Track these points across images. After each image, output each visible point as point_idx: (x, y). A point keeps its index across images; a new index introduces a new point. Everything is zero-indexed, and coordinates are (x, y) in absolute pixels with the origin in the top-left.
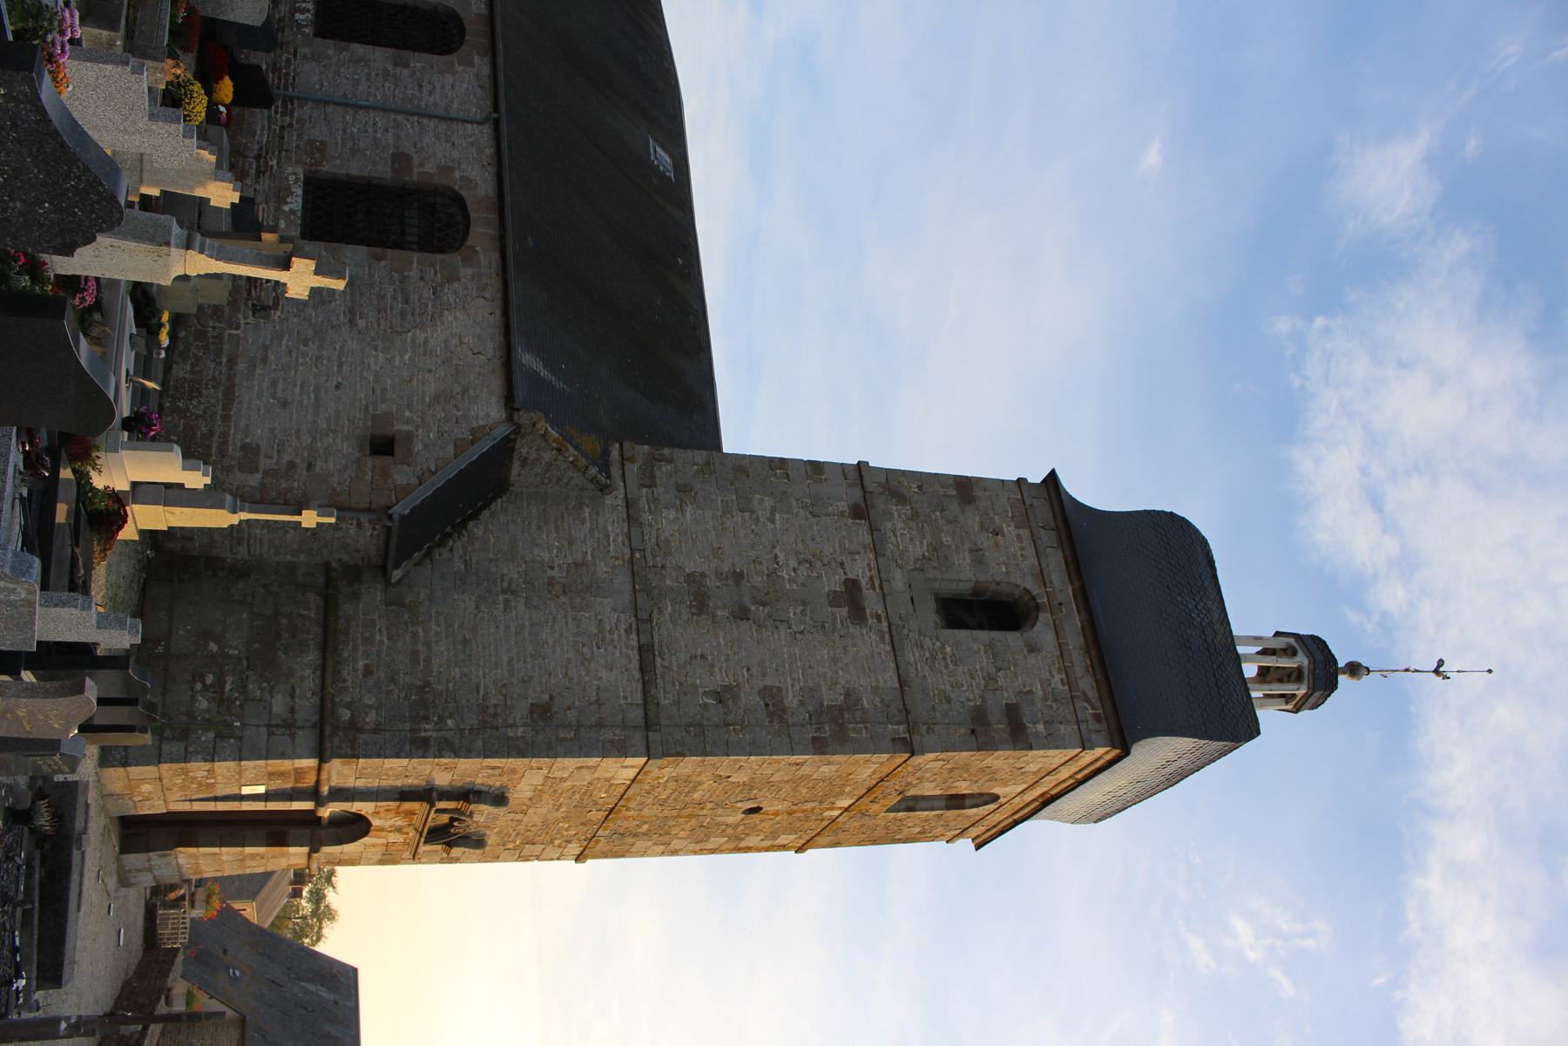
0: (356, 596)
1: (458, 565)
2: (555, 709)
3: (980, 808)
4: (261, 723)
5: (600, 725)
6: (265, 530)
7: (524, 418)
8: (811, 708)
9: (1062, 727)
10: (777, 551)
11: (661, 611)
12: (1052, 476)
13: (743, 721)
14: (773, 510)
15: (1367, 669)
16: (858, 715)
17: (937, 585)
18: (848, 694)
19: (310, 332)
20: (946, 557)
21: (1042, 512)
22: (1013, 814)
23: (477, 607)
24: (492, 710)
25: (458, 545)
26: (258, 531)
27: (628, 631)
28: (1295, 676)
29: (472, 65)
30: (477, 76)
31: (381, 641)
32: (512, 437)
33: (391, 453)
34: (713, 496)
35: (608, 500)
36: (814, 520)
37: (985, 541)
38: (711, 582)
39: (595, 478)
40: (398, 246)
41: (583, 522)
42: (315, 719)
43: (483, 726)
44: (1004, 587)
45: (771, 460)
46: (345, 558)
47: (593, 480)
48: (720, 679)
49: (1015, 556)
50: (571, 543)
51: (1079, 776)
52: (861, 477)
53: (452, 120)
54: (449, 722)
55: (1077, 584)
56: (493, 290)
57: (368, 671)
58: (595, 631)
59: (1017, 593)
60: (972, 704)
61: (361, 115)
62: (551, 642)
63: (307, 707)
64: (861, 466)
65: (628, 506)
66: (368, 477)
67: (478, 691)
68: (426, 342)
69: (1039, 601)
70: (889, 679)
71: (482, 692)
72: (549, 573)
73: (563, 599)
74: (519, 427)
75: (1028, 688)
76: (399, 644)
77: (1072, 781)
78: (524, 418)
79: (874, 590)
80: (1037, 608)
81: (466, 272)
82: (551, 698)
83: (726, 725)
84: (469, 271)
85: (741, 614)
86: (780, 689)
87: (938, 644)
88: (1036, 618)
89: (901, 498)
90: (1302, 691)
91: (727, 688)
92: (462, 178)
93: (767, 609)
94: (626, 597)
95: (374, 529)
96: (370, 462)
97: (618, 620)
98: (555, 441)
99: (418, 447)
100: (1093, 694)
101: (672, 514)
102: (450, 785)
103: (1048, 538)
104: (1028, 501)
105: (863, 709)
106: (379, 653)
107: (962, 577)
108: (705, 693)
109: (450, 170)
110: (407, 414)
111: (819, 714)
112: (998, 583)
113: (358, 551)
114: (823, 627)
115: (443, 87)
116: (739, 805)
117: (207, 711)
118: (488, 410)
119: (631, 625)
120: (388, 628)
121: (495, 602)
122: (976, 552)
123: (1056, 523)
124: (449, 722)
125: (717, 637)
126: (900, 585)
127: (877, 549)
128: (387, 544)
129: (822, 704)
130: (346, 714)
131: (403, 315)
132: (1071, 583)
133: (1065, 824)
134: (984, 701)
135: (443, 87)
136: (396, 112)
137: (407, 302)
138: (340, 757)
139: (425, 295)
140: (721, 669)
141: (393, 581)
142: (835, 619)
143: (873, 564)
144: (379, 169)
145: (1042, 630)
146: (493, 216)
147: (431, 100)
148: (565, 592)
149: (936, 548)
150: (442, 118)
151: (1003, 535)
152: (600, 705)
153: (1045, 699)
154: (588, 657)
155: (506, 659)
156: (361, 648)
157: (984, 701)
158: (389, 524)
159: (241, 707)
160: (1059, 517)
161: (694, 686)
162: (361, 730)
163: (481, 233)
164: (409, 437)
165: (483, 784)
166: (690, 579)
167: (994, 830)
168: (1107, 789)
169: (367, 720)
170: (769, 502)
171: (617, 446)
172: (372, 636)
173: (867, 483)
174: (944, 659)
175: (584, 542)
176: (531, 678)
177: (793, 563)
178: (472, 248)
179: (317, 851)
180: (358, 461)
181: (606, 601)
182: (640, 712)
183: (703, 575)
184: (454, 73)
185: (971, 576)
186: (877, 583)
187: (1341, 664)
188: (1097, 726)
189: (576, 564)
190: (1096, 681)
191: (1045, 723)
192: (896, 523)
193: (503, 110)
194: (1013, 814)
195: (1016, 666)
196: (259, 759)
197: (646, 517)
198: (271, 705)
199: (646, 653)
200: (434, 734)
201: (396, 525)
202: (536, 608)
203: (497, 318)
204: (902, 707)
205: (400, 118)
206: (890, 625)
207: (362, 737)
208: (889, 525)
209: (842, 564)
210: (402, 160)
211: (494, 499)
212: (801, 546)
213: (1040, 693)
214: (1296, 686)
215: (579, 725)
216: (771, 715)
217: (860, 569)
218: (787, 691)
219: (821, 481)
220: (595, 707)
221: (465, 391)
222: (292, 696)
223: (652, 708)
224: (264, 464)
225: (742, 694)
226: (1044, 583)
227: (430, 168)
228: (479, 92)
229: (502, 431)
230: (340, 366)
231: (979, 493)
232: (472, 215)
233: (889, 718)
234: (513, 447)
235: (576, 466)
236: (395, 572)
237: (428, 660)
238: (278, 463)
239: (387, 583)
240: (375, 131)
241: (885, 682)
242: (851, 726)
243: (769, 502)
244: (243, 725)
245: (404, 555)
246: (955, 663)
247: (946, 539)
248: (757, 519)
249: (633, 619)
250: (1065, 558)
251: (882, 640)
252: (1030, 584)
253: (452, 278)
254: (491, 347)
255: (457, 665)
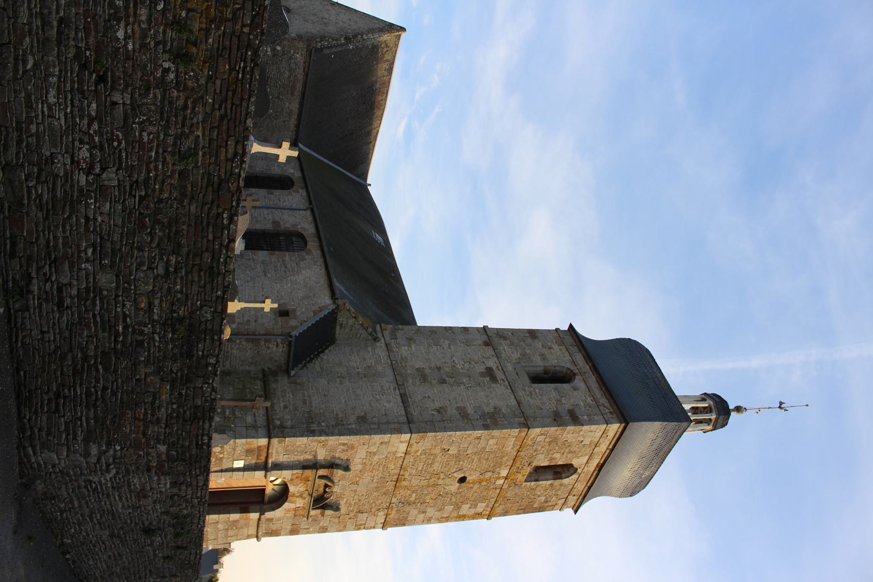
0: (276, 381)
1: (318, 369)
2: (367, 418)
3: (570, 478)
4: (242, 425)
5: (388, 423)
6: (238, 351)
7: (340, 302)
8: (480, 414)
9: (595, 417)
10: (454, 358)
11: (407, 382)
12: (571, 326)
13: (450, 419)
14: (450, 345)
15: (745, 408)
16: (501, 415)
17: (527, 369)
18: (495, 408)
19: (249, 279)
20: (529, 358)
21: (569, 340)
22: (587, 483)
23: (328, 383)
24: (340, 419)
25: (317, 362)
26: (235, 352)
27: (395, 389)
28: (707, 410)
29: (299, 192)
30: (301, 196)
31: (289, 397)
32: (336, 311)
33: (288, 315)
34: (423, 341)
35: (378, 344)
36: (468, 348)
37: (545, 351)
38: (427, 371)
39: (371, 333)
40: (281, 250)
41: (369, 352)
42: (265, 424)
43: (337, 425)
44: (558, 368)
45: (445, 328)
46: (271, 366)
47: (370, 334)
48: (437, 405)
49: (560, 356)
50: (365, 360)
51: (611, 447)
52: (486, 331)
53: (294, 209)
54: (323, 424)
55: (590, 364)
56: (320, 261)
57: (285, 407)
58: (380, 390)
59: (564, 370)
60: (552, 410)
61: (257, 210)
62: (362, 394)
63: (261, 420)
64: (485, 328)
65: (387, 345)
66: (280, 323)
67: (334, 413)
68: (296, 280)
69: (575, 372)
70: (513, 402)
71: (335, 413)
72: (357, 370)
73: (365, 379)
74: (338, 306)
75: (576, 403)
76: (297, 397)
77: (608, 451)
78: (340, 302)
79: (499, 370)
80: (574, 374)
81: (308, 257)
82: (365, 414)
83: (444, 421)
84: (310, 257)
85: (443, 381)
86: (464, 407)
87: (532, 389)
88: (575, 378)
89: (505, 338)
90: (713, 417)
91: (441, 408)
92: (301, 228)
93: (454, 379)
94: (392, 377)
95: (284, 347)
96: (280, 319)
97: (390, 386)
98: (354, 313)
99: (298, 313)
100: (607, 404)
101: (406, 348)
102: (325, 460)
103: (574, 349)
104: (562, 336)
105: (503, 413)
106: (289, 401)
107: (538, 364)
108: (432, 410)
109: (297, 225)
110: (292, 303)
111: (483, 416)
112: (555, 367)
113: (276, 361)
114: (479, 384)
115: (288, 200)
116: (455, 475)
117: (220, 421)
118: (326, 300)
119: (395, 387)
120: (291, 392)
121: (336, 381)
122: (542, 355)
123: (576, 342)
124: (323, 424)
125: (434, 390)
126: (511, 368)
127: (498, 356)
128: (289, 357)
129: (484, 412)
130: (278, 423)
131: (285, 272)
132: (588, 364)
133: (616, 498)
134: (557, 408)
135: (288, 200)
136: (271, 208)
137: (286, 268)
138: (277, 437)
139: (293, 265)
140: (437, 401)
141: (291, 375)
142: (484, 382)
143: (497, 362)
144: (269, 226)
145: (578, 381)
146: (316, 239)
147: (284, 204)
148: (365, 377)
149: (524, 355)
150: (290, 209)
151: (553, 349)
152: (387, 416)
153: (585, 407)
154: (379, 398)
155: (343, 401)
156: (281, 399)
157: (557, 408)
158: (291, 339)
159: (234, 420)
160: (577, 341)
161: (427, 408)
162: (285, 428)
163: (313, 245)
164: (295, 310)
165: (339, 458)
166: (418, 370)
167: (581, 498)
168: (629, 466)
169: (288, 424)
170: (447, 342)
171: (379, 326)
172: (285, 395)
173: (488, 333)
174: (536, 394)
175: (370, 359)
176: (355, 407)
177: (462, 362)
178: (310, 250)
179: (264, 514)
180: (275, 319)
181: (383, 379)
182: (405, 418)
183: (423, 368)
184: (292, 195)
185: (542, 364)
186: (500, 368)
187: (731, 407)
188: (612, 416)
189: (368, 367)
190: (608, 399)
191: (587, 416)
192: (505, 348)
193: (313, 203)
194: (587, 483)
195: (569, 395)
196: (243, 438)
197: (395, 349)
198: (246, 420)
199: (404, 397)
200: (317, 428)
201: (293, 340)
202: (354, 383)
203: (323, 271)
204: (520, 412)
205: (273, 210)
206: (509, 382)
207: (286, 430)
208: (502, 348)
209: (483, 362)
210: (276, 223)
211: (330, 346)
212: (464, 357)
213: (582, 404)
214: (710, 414)
215: (379, 423)
216: (463, 417)
217: (492, 363)
218: (468, 408)
219: (468, 334)
220: (384, 417)
221: (314, 295)
222: (255, 416)
223: (409, 415)
224: (237, 320)
225: (448, 410)
226: (576, 365)
227: (288, 225)
228: (303, 201)
229: (333, 307)
230: (263, 289)
231: (539, 335)
232: (307, 239)
233: (515, 416)
234: (336, 317)
235: (363, 327)
236: (292, 372)
237: (310, 402)
238: (243, 320)
239: (289, 376)
240: (264, 215)
241: (511, 403)
242: (499, 419)
243: (447, 342)
244: (235, 426)
245: (295, 365)
246: (541, 395)
247: (528, 352)
248: (443, 348)
249: (396, 385)
250: (583, 356)
251: (507, 388)
252: (569, 366)
253: (303, 259)
254: (323, 280)
255: (322, 403)
